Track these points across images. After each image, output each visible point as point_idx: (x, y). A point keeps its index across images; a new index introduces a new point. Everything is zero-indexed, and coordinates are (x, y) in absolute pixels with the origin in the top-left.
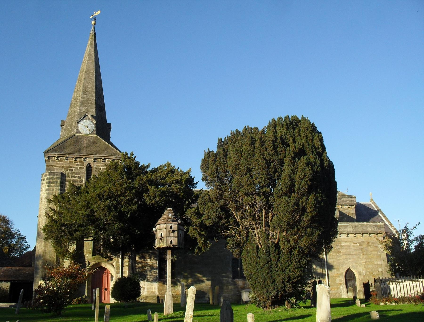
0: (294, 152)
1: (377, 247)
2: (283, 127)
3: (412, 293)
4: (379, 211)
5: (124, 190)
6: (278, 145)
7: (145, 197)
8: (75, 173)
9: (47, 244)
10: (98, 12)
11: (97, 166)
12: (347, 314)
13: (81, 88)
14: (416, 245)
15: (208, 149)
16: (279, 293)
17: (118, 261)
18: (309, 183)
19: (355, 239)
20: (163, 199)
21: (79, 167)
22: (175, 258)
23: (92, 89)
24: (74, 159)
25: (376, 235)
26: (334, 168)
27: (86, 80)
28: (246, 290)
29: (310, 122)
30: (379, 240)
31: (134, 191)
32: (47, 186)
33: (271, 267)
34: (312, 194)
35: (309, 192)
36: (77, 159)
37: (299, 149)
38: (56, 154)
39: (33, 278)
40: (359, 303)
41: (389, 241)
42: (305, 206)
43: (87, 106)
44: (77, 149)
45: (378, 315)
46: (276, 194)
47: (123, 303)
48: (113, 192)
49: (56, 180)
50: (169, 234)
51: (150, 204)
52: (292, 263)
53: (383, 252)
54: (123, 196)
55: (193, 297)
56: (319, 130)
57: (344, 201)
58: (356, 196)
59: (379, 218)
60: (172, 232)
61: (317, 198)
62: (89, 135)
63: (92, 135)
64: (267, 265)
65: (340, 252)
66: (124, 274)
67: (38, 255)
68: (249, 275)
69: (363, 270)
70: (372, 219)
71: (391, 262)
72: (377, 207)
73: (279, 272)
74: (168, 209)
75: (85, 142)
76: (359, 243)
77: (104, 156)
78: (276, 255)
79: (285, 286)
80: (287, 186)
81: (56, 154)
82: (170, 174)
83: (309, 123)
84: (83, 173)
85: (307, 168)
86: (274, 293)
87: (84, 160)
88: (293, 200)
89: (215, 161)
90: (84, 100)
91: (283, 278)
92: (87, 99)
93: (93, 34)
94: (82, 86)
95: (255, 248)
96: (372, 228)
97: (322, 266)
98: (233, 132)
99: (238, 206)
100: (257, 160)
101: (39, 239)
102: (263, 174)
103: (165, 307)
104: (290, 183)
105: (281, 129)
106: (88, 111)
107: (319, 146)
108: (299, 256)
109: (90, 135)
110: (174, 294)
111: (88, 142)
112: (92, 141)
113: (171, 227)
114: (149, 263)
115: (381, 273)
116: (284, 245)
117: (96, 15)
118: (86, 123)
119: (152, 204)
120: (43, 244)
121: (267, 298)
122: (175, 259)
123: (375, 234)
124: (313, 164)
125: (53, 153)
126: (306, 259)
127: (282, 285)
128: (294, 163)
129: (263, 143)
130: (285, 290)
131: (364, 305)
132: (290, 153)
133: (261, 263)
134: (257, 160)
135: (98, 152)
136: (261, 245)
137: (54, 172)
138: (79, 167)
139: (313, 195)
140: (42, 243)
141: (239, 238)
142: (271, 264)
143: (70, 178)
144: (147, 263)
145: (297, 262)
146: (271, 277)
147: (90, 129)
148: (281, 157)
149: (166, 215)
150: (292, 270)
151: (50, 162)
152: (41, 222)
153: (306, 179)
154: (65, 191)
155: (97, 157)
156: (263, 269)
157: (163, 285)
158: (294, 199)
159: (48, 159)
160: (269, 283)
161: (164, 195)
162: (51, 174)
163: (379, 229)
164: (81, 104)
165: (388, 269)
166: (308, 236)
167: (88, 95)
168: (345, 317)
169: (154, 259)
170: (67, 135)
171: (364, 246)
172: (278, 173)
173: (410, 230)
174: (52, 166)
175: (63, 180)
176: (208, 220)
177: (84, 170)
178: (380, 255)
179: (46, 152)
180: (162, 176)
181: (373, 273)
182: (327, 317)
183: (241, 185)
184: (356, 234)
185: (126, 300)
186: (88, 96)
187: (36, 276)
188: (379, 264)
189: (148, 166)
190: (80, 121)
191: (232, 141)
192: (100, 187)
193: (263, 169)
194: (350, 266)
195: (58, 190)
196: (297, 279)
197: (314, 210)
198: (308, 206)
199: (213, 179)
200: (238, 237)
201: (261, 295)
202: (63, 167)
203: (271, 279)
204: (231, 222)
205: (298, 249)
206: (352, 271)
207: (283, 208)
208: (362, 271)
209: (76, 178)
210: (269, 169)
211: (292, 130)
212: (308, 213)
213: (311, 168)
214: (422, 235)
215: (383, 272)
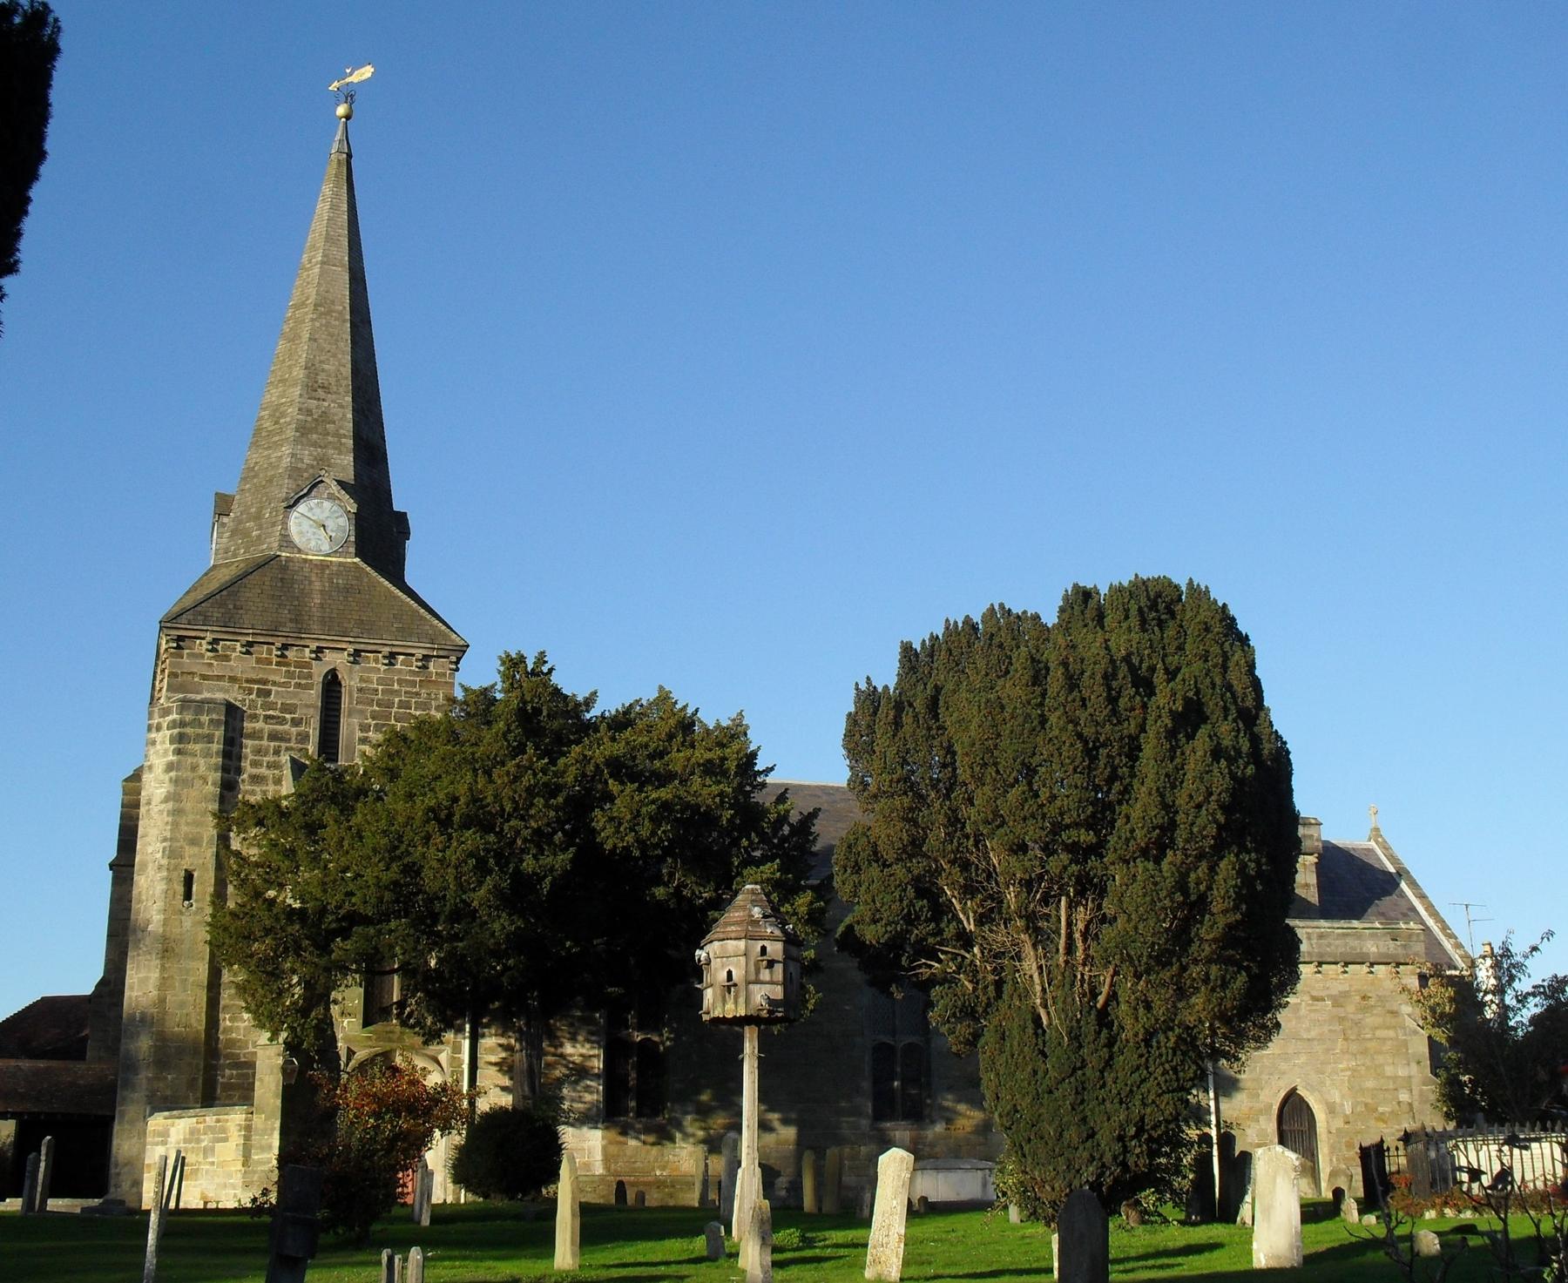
0: (1171, 710)
1: (1394, 1013)
2: (1127, 617)
3: (1526, 1178)
4: (1400, 875)
5: (524, 795)
6: (1120, 688)
7: (598, 822)
8: (279, 706)
9: (172, 977)
10: (363, 70)
12: (1339, 1240)
13: (299, 373)
14: (1538, 1010)
15: (868, 678)
16: (1104, 1173)
17: (457, 1049)
18: (1221, 818)
19: (1317, 981)
20: (664, 832)
21: (293, 682)
22: (668, 1039)
24: (275, 652)
25: (1394, 970)
26: (1289, 760)
27: (315, 340)
28: (925, 1162)
29: (1215, 601)
30: (1409, 991)
31: (560, 800)
33: (1084, 1089)
34: (1229, 853)
35: (1219, 849)
36: (286, 653)
37: (1187, 701)
38: (209, 628)
39: (112, 1106)
40: (1356, 1213)
41: (1441, 994)
42: (1205, 892)
43: (322, 445)
44: (286, 612)
45: (1437, 1241)
46: (1115, 850)
47: (499, 1203)
48: (484, 803)
49: (206, 731)
50: (758, 972)
51: (615, 846)
52: (1151, 1074)
53: (1415, 1032)
54: (522, 818)
55: (904, 1182)
56: (1243, 627)
58: (1320, 820)
59: (1402, 902)
60: (766, 968)
61: (1244, 866)
62: (330, 559)
63: (341, 560)
64: (1072, 1079)
67: (132, 1017)
68: (1008, 1114)
69: (1343, 1097)
70: (1377, 905)
71: (1447, 1069)
72: (1393, 859)
73: (1108, 1104)
74: (748, 887)
75: (317, 586)
76: (1331, 997)
77: (390, 643)
78: (1103, 1047)
79: (1125, 1150)
80: (1154, 828)
81: (209, 628)
82: (680, 738)
83: (1213, 607)
84: (307, 706)
85: (1216, 771)
86: (1089, 1173)
87: (313, 656)
88: (1173, 873)
89: (897, 724)
90: (309, 419)
91: (1121, 1126)
92: (321, 416)
93: (341, 158)
94: (302, 361)
95: (1030, 1025)
96: (1381, 943)
98: (952, 623)
99: (971, 879)
100: (1057, 738)
101: (138, 955)
102: (1076, 787)
103: (739, 1216)
104: (1163, 818)
105: (1120, 627)
106: (323, 461)
107: (1245, 688)
108: (1174, 1054)
109: (334, 559)
110: (661, 1175)
111: (327, 584)
112: (341, 581)
113: (764, 949)
114: (571, 1055)
115: (1405, 1108)
116: (1137, 1019)
117: (356, 81)
118: (317, 511)
119: (623, 847)
120: (155, 975)
121: (1068, 1190)
122: (668, 1043)
123: (1389, 964)
124: (1232, 753)
125: (195, 627)
126: (1197, 1064)
127: (1117, 1147)
128: (1173, 750)
129: (1072, 682)
130: (1124, 1165)
131: (1371, 1219)
132: (1160, 717)
133: (1052, 1074)
134: (1057, 738)
135: (367, 628)
136: (1048, 1013)
137: (199, 697)
138: (293, 682)
139: (1232, 858)
140: (149, 971)
141: (970, 986)
142: (1083, 1078)
143: (260, 725)
144: (562, 1056)
145: (1168, 1073)
146: (1084, 1120)
147: (333, 535)
148: (1131, 727)
149: (744, 908)
150: (1152, 1097)
151: (185, 659)
152: (147, 892)
153: (1213, 806)
154: (239, 775)
155: (362, 647)
156: (1057, 1094)
157: (622, 1139)
158: (1174, 868)
160: (1076, 1140)
161: (668, 817)
162: (189, 707)
163: (1404, 946)
164: (298, 434)
165: (1433, 1097)
166: (1213, 990)
167: (324, 400)
168: (1333, 1249)
170: (243, 556)
171: (1351, 1008)
172: (1121, 784)
173: (1518, 959)
174: (190, 677)
175: (234, 730)
176: (873, 927)
177: (314, 695)
178: (1405, 1044)
179: (168, 623)
180: (653, 746)
181: (1381, 1109)
182: (1291, 1247)
183: (997, 820)
184: (1320, 964)
185: (510, 1192)
186: (326, 404)
187: (124, 1099)
188: (1400, 1074)
189: (589, 702)
190: (297, 502)
191: (951, 654)
192: (422, 776)
193: (1075, 770)
194: (1298, 1080)
196: (1166, 1127)
197: (1236, 908)
198: (1215, 892)
199: (891, 786)
200: (966, 983)
201: (1048, 1178)
202: (233, 679)
203: (1083, 1127)
204: (947, 935)
205: (1177, 1031)
206: (1304, 1100)
207: (1139, 900)
208: (1338, 1100)
210: (1095, 769)
211: (1156, 628)
212: (1213, 915)
213: (1226, 771)
214: (1561, 975)
215: (1416, 1105)
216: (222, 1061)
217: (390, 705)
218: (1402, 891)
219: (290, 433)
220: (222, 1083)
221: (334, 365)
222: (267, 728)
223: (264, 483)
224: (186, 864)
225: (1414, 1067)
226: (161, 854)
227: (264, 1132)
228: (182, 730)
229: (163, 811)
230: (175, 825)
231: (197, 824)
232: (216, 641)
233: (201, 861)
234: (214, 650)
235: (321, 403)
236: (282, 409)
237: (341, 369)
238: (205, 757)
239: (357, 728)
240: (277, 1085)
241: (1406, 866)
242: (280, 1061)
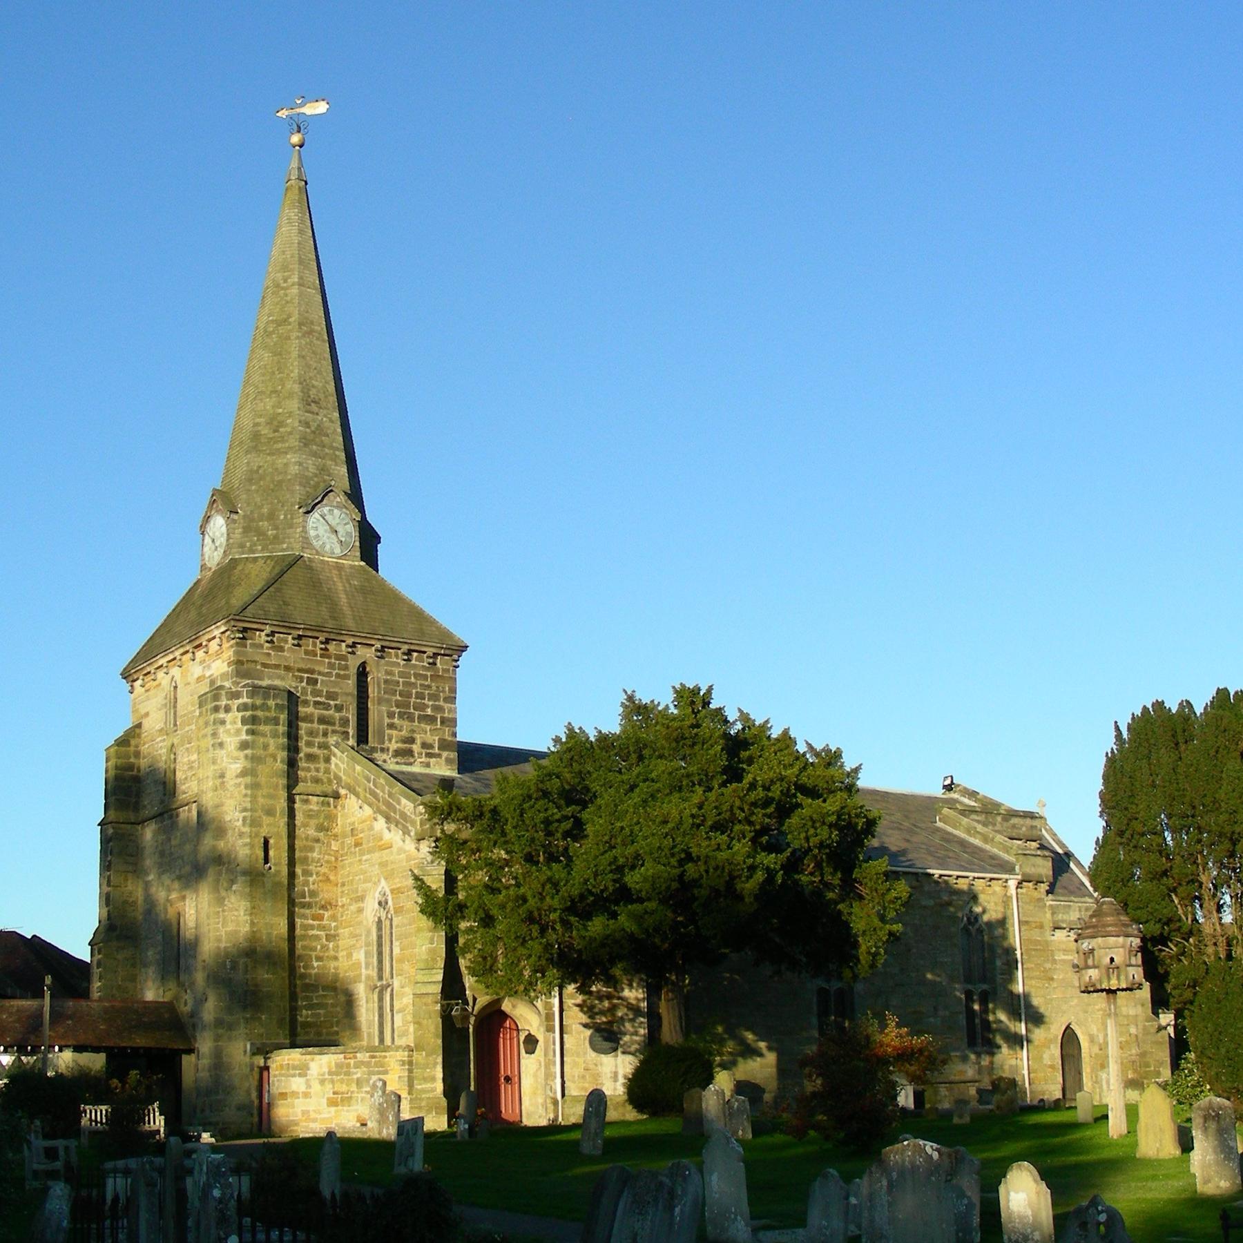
8: (324, 694)
11: (387, 673)
21: (334, 672)
23: (327, 393)
32: (244, 733)
36: (328, 647)
38: (269, 622)
43: (321, 456)
57: (1014, 826)
62: (341, 561)
65: (1052, 979)
69: (1098, 1030)
81: (269, 622)
84: (347, 694)
90: (308, 430)
94: (295, 374)
101: (223, 911)
109: (344, 562)
138: (334, 672)
147: (343, 539)
155: (387, 644)
162: (258, 692)
167: (317, 414)
174: (253, 665)
177: (351, 684)
194: (1073, 1017)
202: (287, 668)
209: (327, 710)
215: (1140, 1035)
216: (300, 1003)
217: (410, 696)
219: (293, 442)
220: (301, 1022)
221: (321, 382)
223: (272, 486)
224: (264, 832)
225: (1140, 1009)
227: (426, 1066)
230: (254, 798)
232: (273, 633)
233: (276, 830)
234: (272, 642)
235: (315, 417)
237: (327, 386)
238: (274, 737)
239: (385, 715)
240: (436, 1028)
241: (1070, 849)
242: (438, 1007)
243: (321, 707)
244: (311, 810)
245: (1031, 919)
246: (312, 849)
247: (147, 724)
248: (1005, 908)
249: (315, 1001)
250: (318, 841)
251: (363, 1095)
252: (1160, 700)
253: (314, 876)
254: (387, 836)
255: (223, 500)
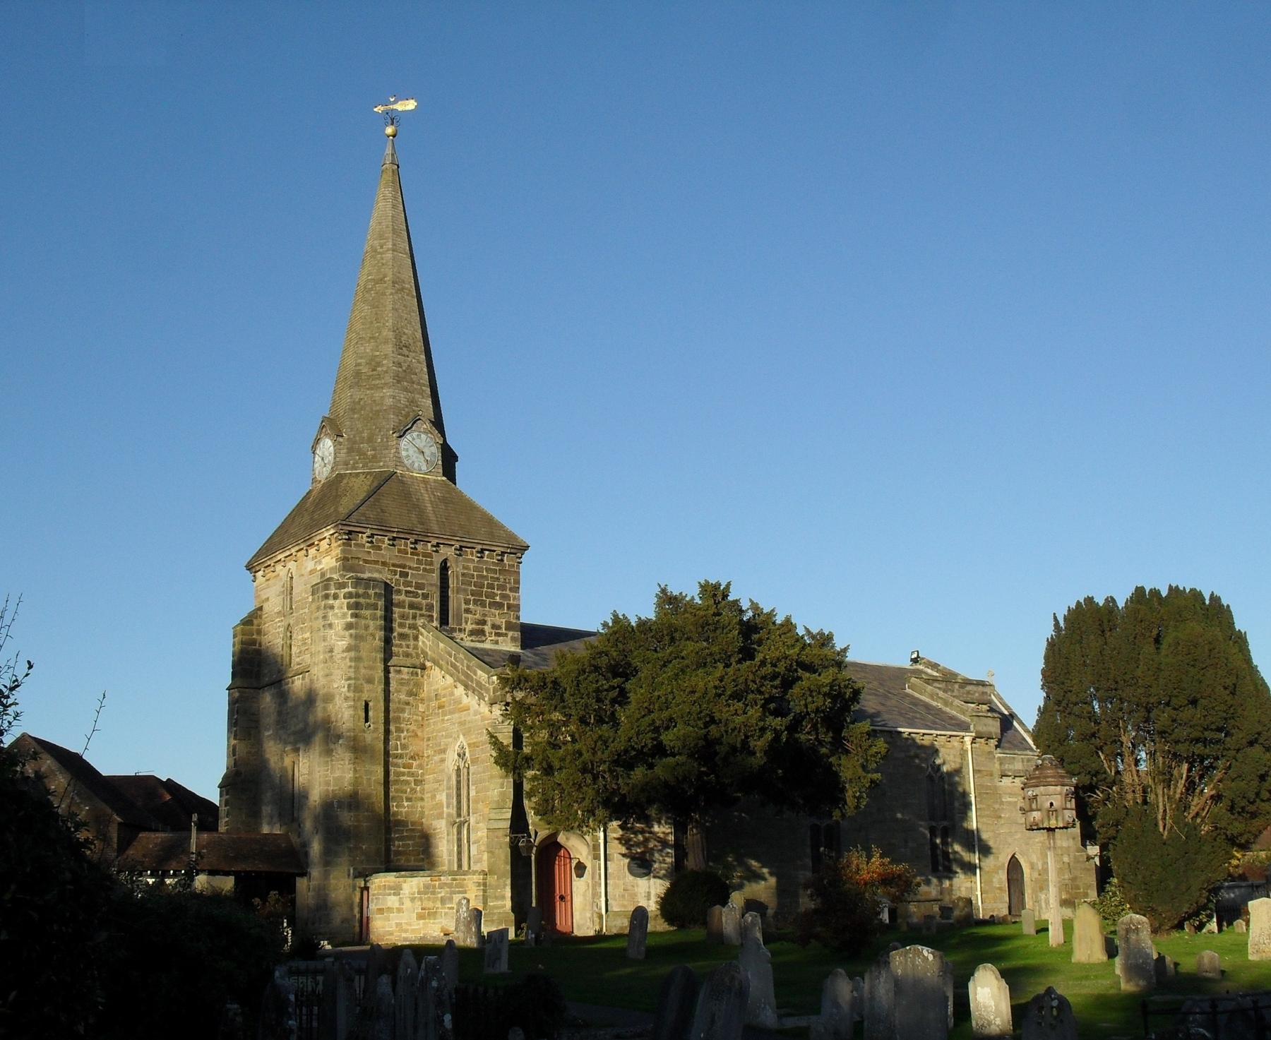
11: (464, 568)
13: (387, 333)
36: (417, 546)
38: (370, 526)
49: (372, 601)
57: (968, 693)
63: (434, 478)
65: (1000, 817)
66: (609, 861)
72: (1007, 708)
81: (370, 526)
84: (431, 585)
90: (400, 369)
94: (389, 324)
97: (970, 848)
101: (332, 761)
109: (430, 477)
125: (361, 525)
143: (402, 597)
147: (429, 459)
154: (392, 633)
159: (346, 539)
162: (361, 584)
167: (408, 356)
169: (666, 823)
174: (357, 561)
177: (435, 577)
186: (409, 359)
188: (1064, 846)
195: (381, 630)
202: (384, 564)
208: (1035, 861)
216: (393, 835)
218: (1015, 727)
219: (388, 379)
220: (394, 851)
222: (408, 599)
224: (365, 696)
226: (346, 689)
228: (358, 600)
229: (346, 657)
230: (357, 668)
231: (371, 668)
232: (372, 536)
236: (378, 360)
243: (412, 595)
244: (402, 679)
245: (983, 769)
246: (403, 711)
247: (266, 607)
248: (962, 759)
249: (405, 834)
250: (408, 704)
251: (446, 910)
252: (1090, 596)
253: (405, 732)
254: (465, 700)
255: (331, 426)
